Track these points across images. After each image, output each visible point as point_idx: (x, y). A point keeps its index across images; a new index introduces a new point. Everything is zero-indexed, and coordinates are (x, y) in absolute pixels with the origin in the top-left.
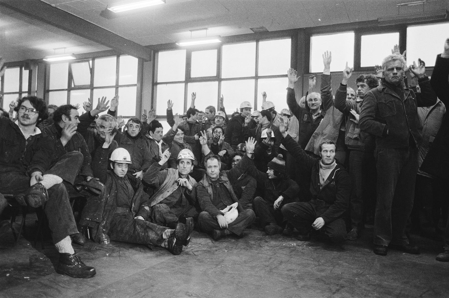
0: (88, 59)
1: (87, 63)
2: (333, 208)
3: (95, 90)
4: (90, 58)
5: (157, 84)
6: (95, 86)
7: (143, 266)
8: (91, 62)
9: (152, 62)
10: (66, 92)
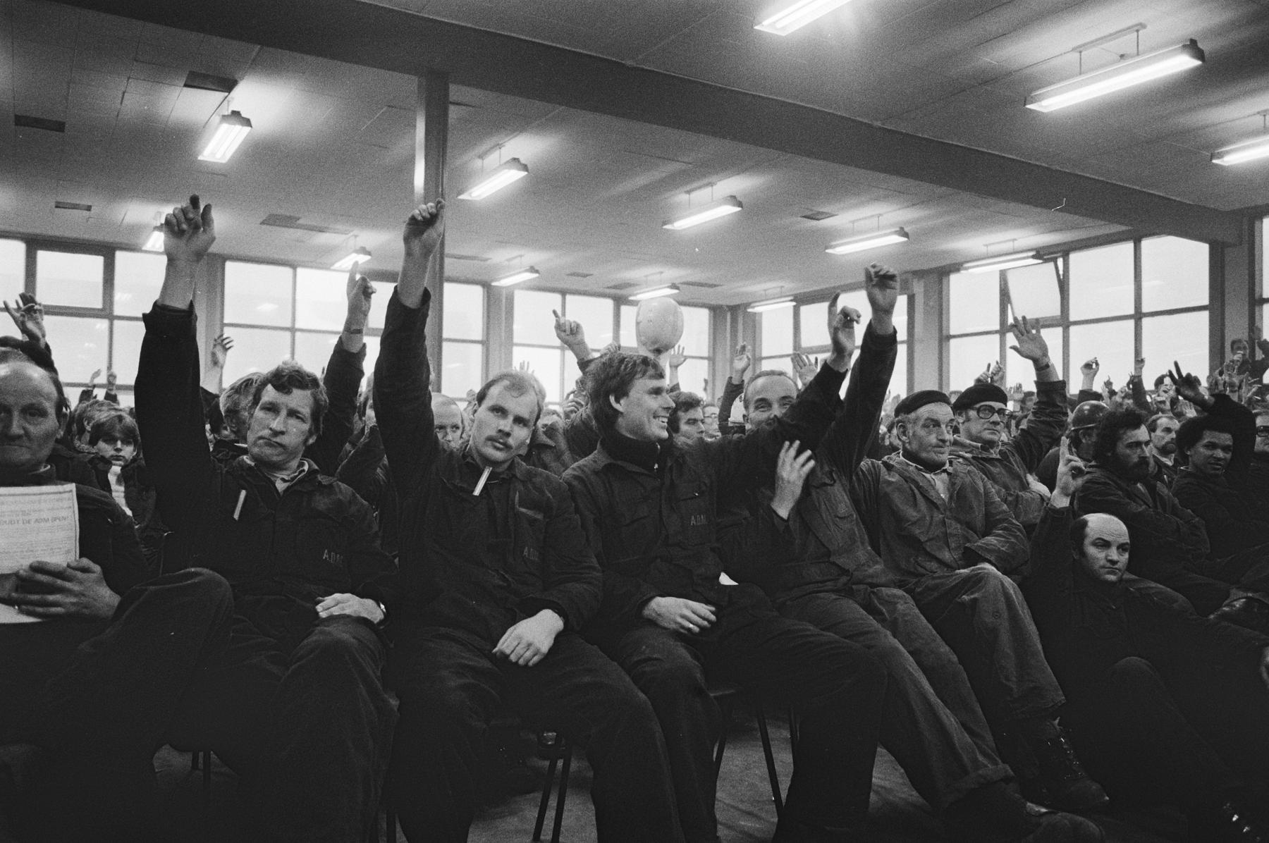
0: (1053, 256)
1: (1051, 265)
2: (1148, 666)
3: (1073, 329)
5: (949, 337)
6: (1072, 319)
7: (106, 224)
8: (1060, 262)
9: (1246, 246)
10: (997, 337)
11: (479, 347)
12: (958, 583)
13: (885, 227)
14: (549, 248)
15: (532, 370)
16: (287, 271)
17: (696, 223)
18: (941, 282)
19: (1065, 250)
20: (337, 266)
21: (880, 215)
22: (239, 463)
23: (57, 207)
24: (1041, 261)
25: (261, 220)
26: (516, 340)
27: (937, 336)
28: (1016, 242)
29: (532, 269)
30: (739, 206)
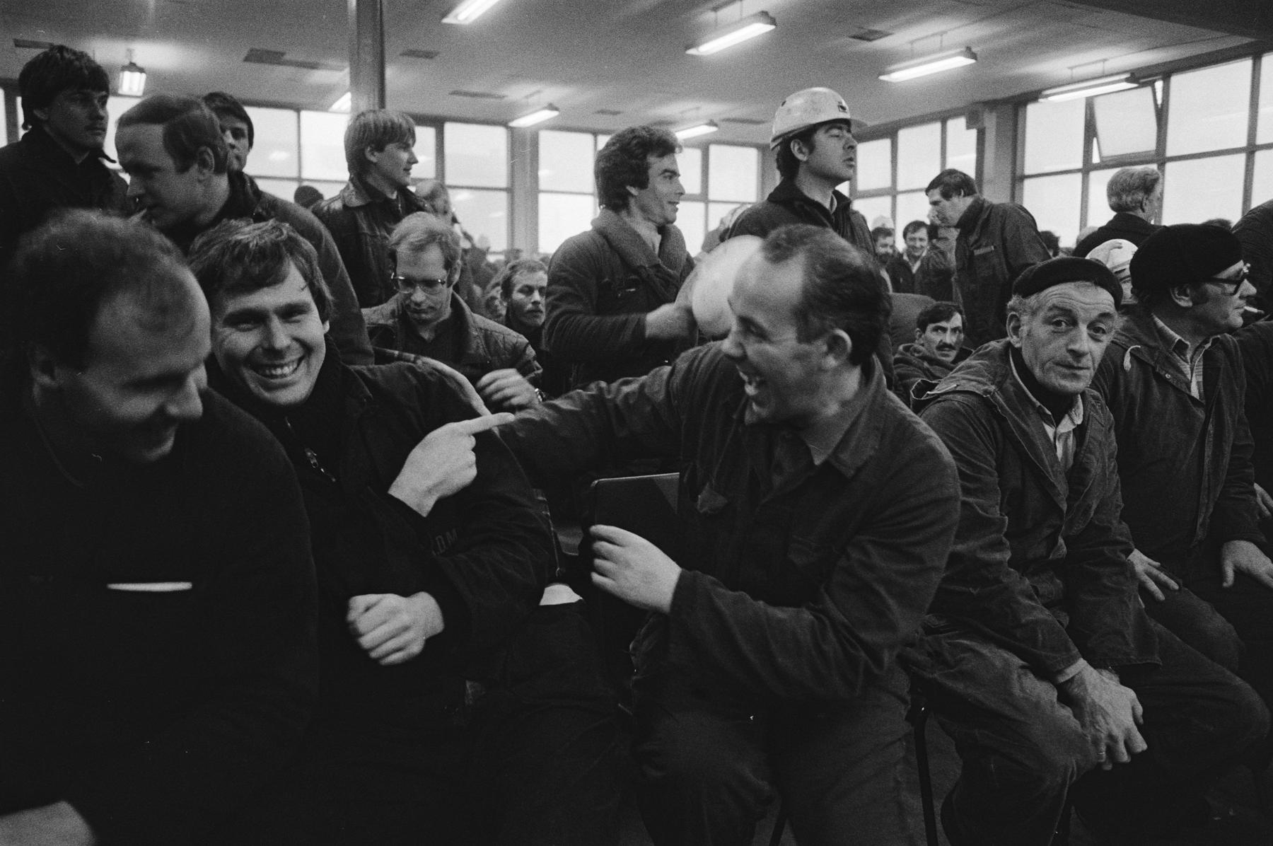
0: (1150, 79)
1: (1148, 90)
4: (1157, 75)
5: (1024, 178)
8: (1159, 85)
10: (1079, 176)
11: (504, 195)
12: (942, 440)
13: (950, 48)
14: (568, 81)
15: (946, 235)
16: (289, 115)
17: (947, 68)
18: (1016, 115)
19: (1167, 72)
20: (335, 107)
21: (945, 32)
22: (639, 319)
23: (17, 46)
24: (1135, 85)
25: (243, 57)
26: (542, 186)
27: (1008, 175)
28: (1107, 63)
29: (551, 107)
30: (771, 24)
